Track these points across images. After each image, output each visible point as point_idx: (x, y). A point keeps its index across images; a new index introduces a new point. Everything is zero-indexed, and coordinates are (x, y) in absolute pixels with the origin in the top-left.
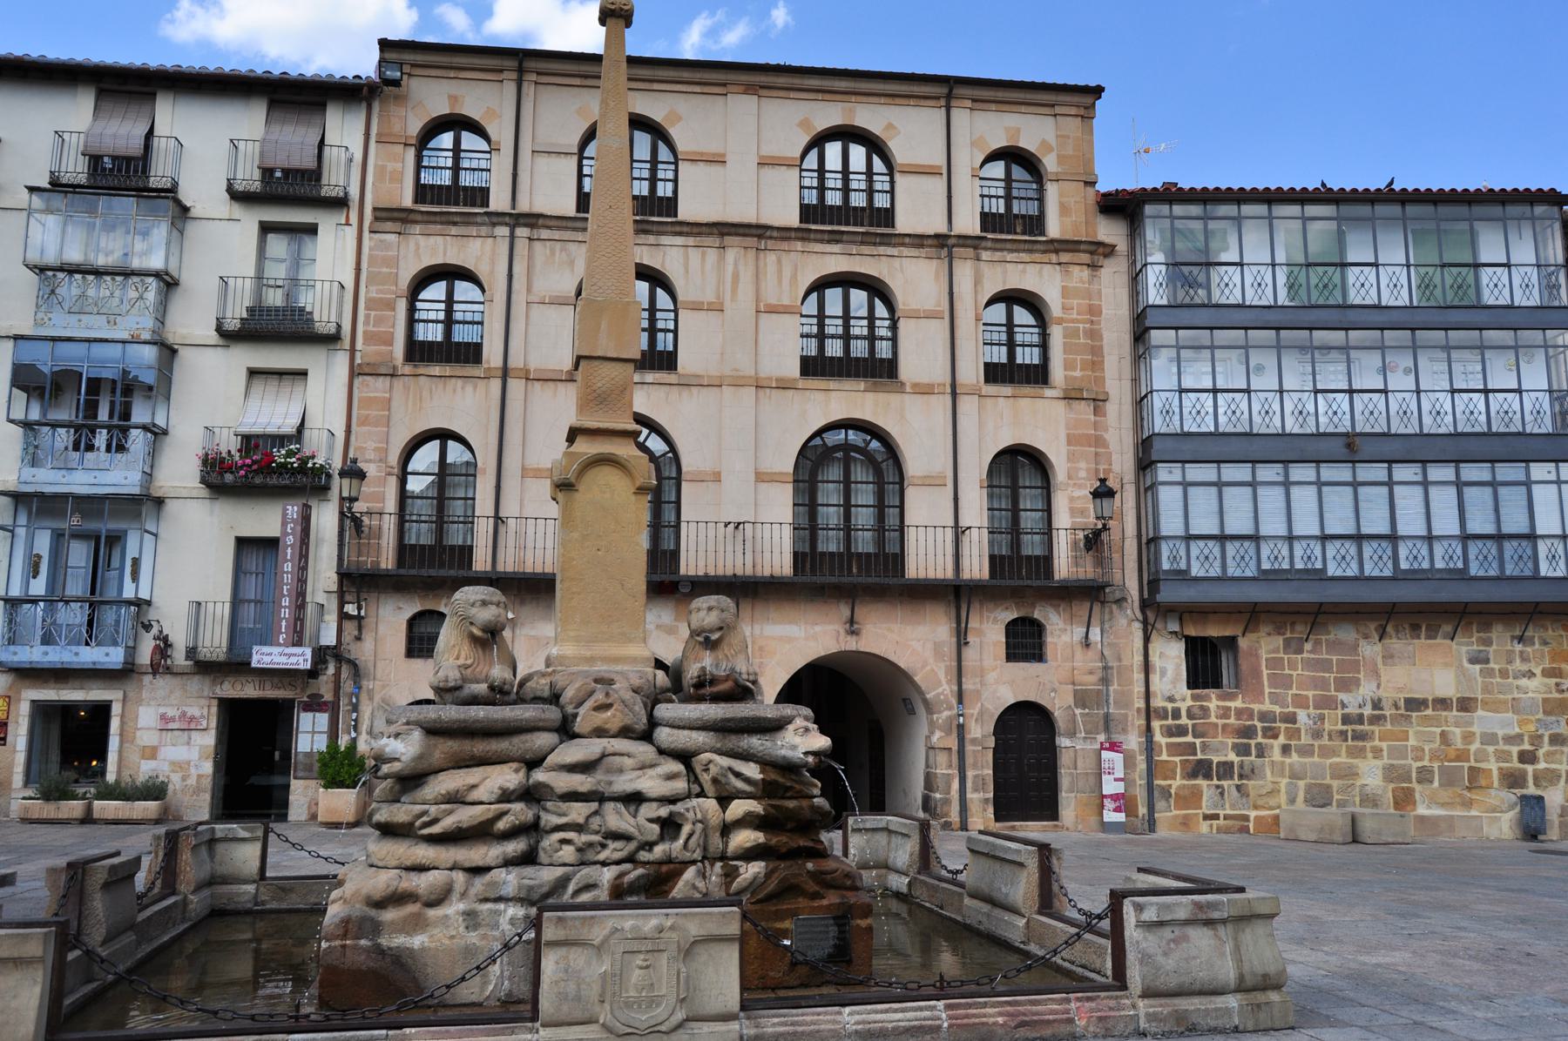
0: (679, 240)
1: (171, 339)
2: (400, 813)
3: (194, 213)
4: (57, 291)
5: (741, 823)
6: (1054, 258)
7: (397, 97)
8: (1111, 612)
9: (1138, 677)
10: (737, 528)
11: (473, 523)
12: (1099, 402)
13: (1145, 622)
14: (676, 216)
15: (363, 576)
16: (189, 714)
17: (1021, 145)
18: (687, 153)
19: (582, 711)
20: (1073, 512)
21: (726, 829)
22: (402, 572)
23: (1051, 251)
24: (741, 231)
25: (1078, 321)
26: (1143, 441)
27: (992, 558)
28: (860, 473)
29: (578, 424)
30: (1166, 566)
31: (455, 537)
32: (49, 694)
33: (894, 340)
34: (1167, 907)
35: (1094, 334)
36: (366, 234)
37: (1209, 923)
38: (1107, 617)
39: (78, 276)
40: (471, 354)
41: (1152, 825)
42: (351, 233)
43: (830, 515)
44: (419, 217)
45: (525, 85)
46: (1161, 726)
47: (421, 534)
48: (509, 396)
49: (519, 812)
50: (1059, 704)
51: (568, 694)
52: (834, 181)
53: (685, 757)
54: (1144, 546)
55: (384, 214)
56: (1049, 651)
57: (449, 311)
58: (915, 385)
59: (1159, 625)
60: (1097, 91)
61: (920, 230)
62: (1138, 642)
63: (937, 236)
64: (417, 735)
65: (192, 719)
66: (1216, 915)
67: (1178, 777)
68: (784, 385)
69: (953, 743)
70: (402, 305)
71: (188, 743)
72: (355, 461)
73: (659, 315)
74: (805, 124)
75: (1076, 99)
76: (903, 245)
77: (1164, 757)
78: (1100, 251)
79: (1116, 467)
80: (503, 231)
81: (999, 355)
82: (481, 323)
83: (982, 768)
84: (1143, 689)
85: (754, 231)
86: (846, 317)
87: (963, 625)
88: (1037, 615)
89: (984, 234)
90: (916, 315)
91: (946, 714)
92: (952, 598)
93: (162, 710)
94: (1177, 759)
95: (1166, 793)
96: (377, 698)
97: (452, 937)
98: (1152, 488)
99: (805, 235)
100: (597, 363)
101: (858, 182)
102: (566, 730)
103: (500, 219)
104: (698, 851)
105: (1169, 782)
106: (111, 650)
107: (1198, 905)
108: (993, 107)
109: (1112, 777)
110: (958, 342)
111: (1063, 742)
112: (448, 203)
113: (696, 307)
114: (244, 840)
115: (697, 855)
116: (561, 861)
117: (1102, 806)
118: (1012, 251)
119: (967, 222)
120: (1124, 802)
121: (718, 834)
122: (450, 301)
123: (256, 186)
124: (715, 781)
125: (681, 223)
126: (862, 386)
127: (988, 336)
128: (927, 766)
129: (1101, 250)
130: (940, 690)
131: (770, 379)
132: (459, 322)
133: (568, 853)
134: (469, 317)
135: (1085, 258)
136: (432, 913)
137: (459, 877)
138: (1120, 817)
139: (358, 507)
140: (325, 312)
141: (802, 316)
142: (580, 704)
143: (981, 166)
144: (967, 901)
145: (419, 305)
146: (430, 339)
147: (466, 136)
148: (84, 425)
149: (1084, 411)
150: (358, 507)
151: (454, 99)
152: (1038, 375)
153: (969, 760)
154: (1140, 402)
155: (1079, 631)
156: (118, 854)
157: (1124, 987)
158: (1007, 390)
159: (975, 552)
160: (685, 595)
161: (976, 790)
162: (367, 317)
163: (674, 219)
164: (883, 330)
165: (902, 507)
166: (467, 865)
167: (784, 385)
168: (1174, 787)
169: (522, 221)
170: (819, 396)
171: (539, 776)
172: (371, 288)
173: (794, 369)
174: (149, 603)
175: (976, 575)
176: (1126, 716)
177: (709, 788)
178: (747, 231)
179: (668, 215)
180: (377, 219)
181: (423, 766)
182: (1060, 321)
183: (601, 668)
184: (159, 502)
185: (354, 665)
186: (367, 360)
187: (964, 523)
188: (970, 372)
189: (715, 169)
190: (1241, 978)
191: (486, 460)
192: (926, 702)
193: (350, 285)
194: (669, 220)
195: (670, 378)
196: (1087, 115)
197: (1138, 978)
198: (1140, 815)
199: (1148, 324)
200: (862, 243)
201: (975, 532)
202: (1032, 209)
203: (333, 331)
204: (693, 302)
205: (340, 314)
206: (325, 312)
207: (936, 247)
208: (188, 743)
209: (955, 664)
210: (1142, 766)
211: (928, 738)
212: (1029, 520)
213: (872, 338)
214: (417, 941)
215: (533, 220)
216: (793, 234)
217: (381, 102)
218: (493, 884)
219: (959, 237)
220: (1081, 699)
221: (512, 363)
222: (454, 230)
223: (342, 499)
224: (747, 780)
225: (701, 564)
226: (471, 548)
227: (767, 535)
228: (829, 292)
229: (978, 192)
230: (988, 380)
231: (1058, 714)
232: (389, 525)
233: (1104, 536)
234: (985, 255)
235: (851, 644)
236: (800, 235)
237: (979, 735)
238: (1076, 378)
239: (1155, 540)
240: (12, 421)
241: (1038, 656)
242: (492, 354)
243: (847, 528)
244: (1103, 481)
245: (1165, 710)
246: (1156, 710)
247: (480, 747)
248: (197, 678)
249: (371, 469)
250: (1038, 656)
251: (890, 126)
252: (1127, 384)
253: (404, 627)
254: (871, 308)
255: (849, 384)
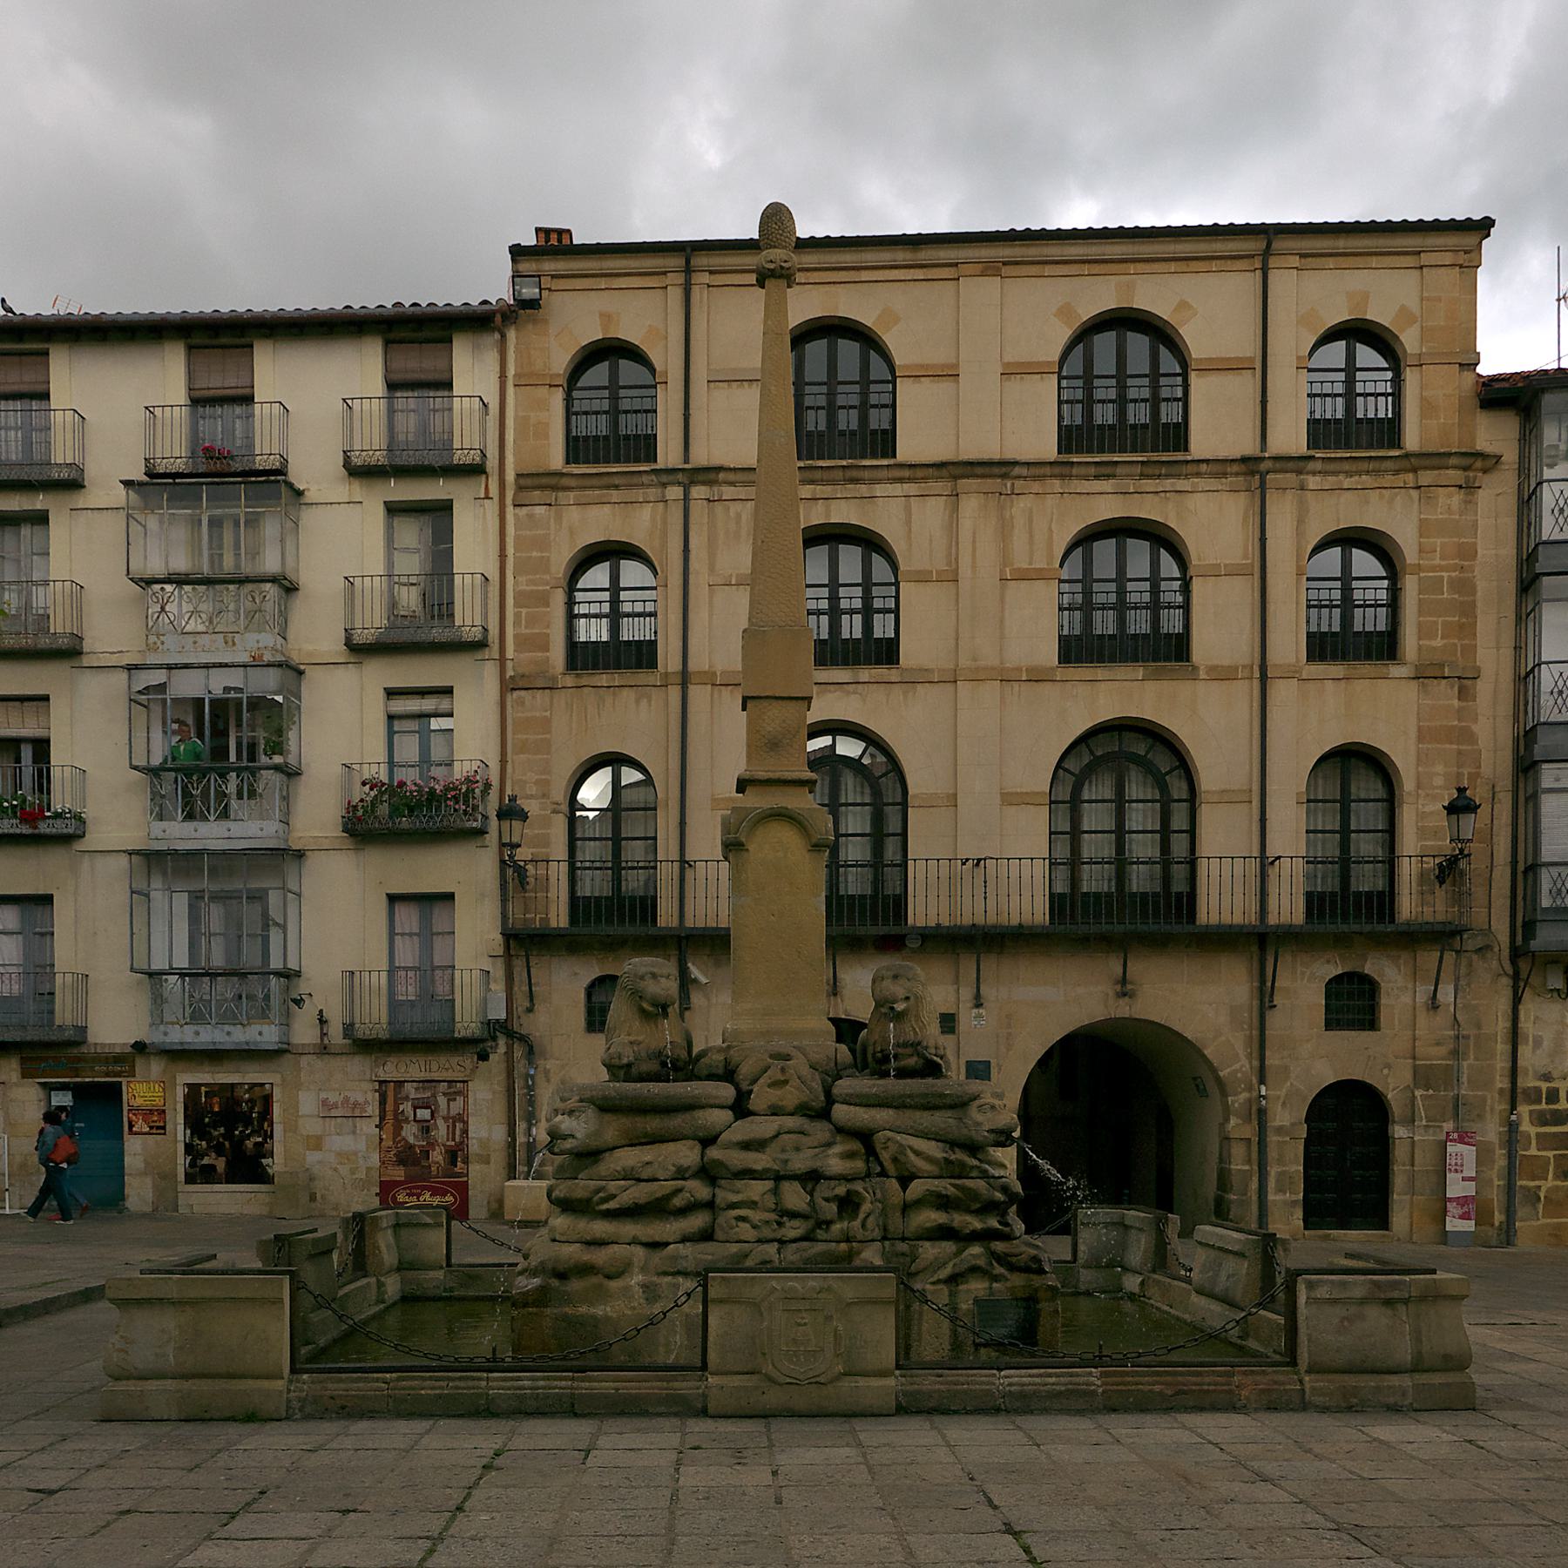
0: (898, 489)
1: (296, 658)
2: (581, 1187)
3: (311, 496)
4: (167, 609)
5: (918, 1203)
6: (1410, 478)
7: (535, 322)
8: (1470, 965)
9: (1502, 1048)
10: (978, 864)
11: (655, 868)
12: (1465, 683)
13: (1516, 977)
14: (894, 456)
15: (529, 936)
16: (352, 1100)
17: (1368, 317)
18: (907, 367)
19: (756, 1088)
20: (1422, 832)
21: (906, 1208)
22: (575, 930)
23: (1407, 471)
24: (979, 470)
25: (1442, 569)
26: (1526, 733)
27: (1309, 896)
28: (1137, 787)
29: (747, 775)
30: (1546, 902)
31: (633, 883)
32: (204, 1076)
33: (1186, 607)
34: (1344, 1284)
35: (1465, 586)
36: (510, 509)
37: (1389, 1302)
38: (1463, 970)
39: (187, 588)
40: (643, 655)
41: (1508, 1234)
42: (491, 507)
43: (1096, 847)
44: (573, 482)
45: (695, 291)
46: (1531, 1112)
47: (594, 885)
48: (691, 709)
49: (698, 1189)
50: (1393, 1085)
51: (745, 1071)
52: (1105, 390)
53: (865, 1137)
54: (1520, 877)
55: (529, 482)
56: (1384, 1017)
57: (615, 602)
58: (1211, 669)
59: (1535, 980)
60: (1484, 226)
61: (1222, 453)
62: (1503, 1003)
63: (1244, 460)
64: (591, 1112)
65: (356, 1104)
66: (1396, 1294)
67: (1550, 1176)
68: (1037, 677)
69: (1249, 1131)
70: (559, 597)
71: (354, 1133)
72: (513, 799)
73: (875, 591)
74: (1065, 312)
75: (1451, 240)
76: (1198, 475)
77: (1533, 1151)
78: (1479, 462)
79: (1486, 770)
80: (675, 492)
81: (1331, 622)
82: (653, 614)
83: (1289, 1160)
84: (1508, 1065)
85: (996, 470)
86: (1121, 578)
87: (1269, 984)
88: (1368, 969)
89: (1311, 453)
90: (1214, 572)
91: (1244, 1096)
92: (1255, 948)
93: (323, 1095)
94: (1550, 1154)
95: (1533, 1197)
96: (555, 1080)
97: (634, 1308)
98: (1533, 799)
99: (1066, 470)
100: (765, 703)
101: (1139, 389)
102: (740, 1108)
103: (671, 478)
104: (877, 1229)
105: (1537, 1183)
106: (266, 1029)
107: (1376, 1284)
108: (1331, 262)
109: (1460, 1176)
110: (1271, 608)
111: (1399, 1132)
112: (607, 461)
113: (922, 578)
114: (426, 1225)
115: (877, 1234)
116: (735, 1237)
117: (1445, 1211)
118: (1349, 474)
119: (1290, 436)
120: (1475, 1207)
121: (898, 1214)
122: (615, 588)
123: (380, 458)
124: (895, 1160)
125: (901, 466)
126: (1140, 673)
127: (1313, 595)
128: (1221, 1160)
129: (1479, 464)
130: (1237, 1066)
131: (1019, 669)
132: (628, 615)
133: (745, 1231)
134: (639, 608)
135: (1455, 476)
136: (614, 1285)
137: (640, 1252)
138: (1469, 1226)
139: (522, 854)
140: (468, 613)
141: (1310, 370)
142: (754, 1081)
143: (1311, 354)
144: (1194, 1298)
145: (579, 596)
146: (593, 639)
147: (624, 364)
148: (211, 769)
149: (1445, 694)
150: (522, 854)
151: (606, 318)
152: (1385, 647)
153: (1272, 1154)
154: (1525, 678)
155: (1423, 991)
156: (315, 1230)
157: (1293, 1363)
158: (1337, 670)
159: (1285, 887)
160: (914, 951)
161: (1281, 1190)
162: (517, 616)
163: (891, 462)
164: (1171, 592)
165: (1192, 833)
166: (644, 1239)
167: (1037, 677)
168: (1543, 1189)
169: (701, 477)
170: (1083, 689)
171: (714, 1153)
172: (520, 579)
173: (1049, 653)
174: (298, 974)
175: (1285, 919)
176: (1484, 1099)
177: (891, 1168)
178: (987, 470)
179: (884, 456)
180: (520, 488)
181: (595, 1144)
182: (1419, 568)
183: (782, 1045)
184: (300, 855)
185: (523, 1039)
186: (521, 671)
187: (1271, 852)
188: (1288, 644)
189: (946, 386)
190: (1418, 1357)
191: (666, 788)
192: (1220, 1082)
193: (494, 576)
194: (885, 462)
195: (892, 674)
196: (1469, 264)
197: (1306, 1355)
198: (1497, 1224)
199: (1539, 569)
200: (1143, 476)
201: (1286, 863)
202: (1384, 409)
203: (479, 637)
204: (919, 572)
205: (485, 616)
206: (468, 613)
207: (1245, 474)
208: (354, 1133)
209: (1255, 1033)
210: (1501, 1162)
211: (1222, 1125)
212: (1365, 846)
213: (1155, 606)
214: (599, 1311)
215: (709, 474)
216: (1047, 470)
217: (517, 330)
218: (675, 1258)
219: (1276, 459)
220: (1423, 1077)
221: (693, 666)
222: (615, 495)
223: (502, 845)
224: (929, 1159)
225: (932, 911)
226: (654, 899)
227: (1014, 874)
228: (1098, 546)
229: (1306, 389)
230: (1311, 657)
231: (1392, 1096)
232: (558, 873)
233: (1462, 864)
234: (1313, 482)
235: (1123, 1010)
236: (1057, 470)
237: (1287, 1123)
238: (1435, 649)
239: (1533, 868)
240: (135, 768)
241: (1368, 1020)
242: (668, 657)
243: (1121, 862)
244: (1461, 790)
245: (1538, 1090)
246: (1526, 1091)
247: (653, 1124)
248: (357, 1059)
249: (531, 806)
250: (1368, 1020)
251: (1183, 305)
252: (1507, 653)
253: (582, 995)
254: (1155, 564)
255: (1123, 671)
